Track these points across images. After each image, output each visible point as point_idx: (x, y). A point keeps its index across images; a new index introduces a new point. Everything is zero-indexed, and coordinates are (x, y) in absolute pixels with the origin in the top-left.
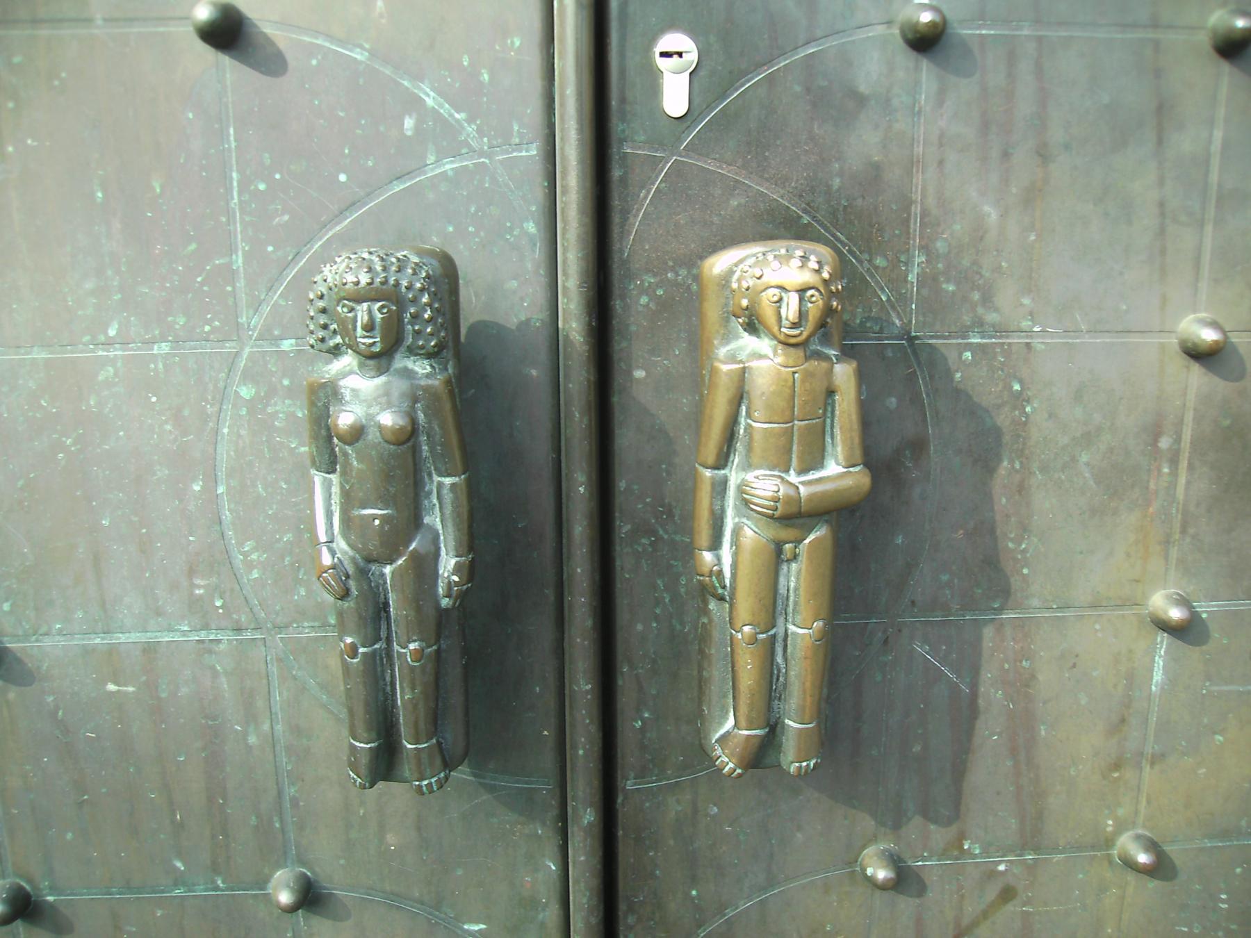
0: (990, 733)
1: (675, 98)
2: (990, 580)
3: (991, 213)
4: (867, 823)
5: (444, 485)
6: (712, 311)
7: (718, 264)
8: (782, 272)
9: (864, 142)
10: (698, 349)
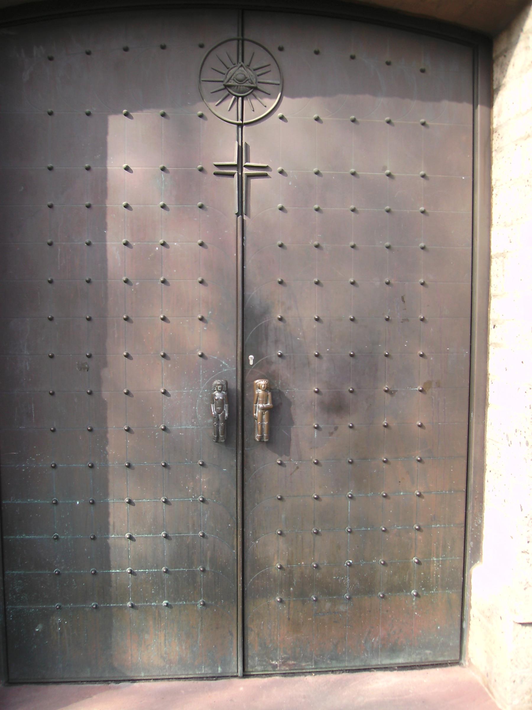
0: (293, 443)
1: (251, 363)
2: (291, 422)
3: (289, 375)
4: (277, 455)
5: (226, 405)
6: (255, 387)
7: (256, 381)
8: (262, 383)
9: (273, 367)
10: (254, 392)
